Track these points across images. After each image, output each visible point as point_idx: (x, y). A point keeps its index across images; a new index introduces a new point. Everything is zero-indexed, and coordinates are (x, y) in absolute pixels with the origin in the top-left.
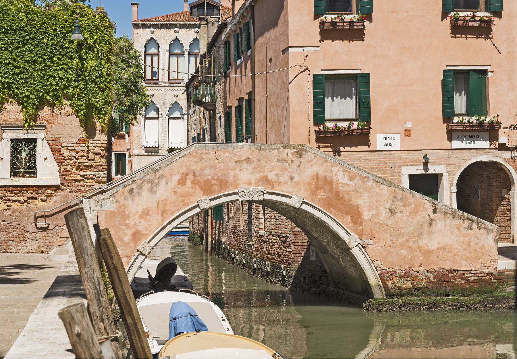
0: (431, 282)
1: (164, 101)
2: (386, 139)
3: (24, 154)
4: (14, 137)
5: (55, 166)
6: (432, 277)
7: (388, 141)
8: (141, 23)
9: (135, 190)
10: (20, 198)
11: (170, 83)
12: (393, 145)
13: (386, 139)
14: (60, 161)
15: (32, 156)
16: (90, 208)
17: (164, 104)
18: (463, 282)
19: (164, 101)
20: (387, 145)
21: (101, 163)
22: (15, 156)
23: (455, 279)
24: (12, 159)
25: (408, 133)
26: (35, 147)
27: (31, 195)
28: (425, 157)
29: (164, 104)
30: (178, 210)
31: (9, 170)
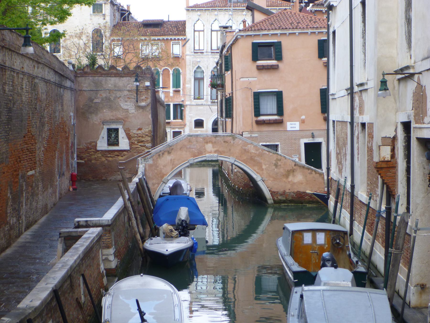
0: (294, 197)
1: (207, 66)
2: (292, 124)
3: (113, 135)
4: (108, 127)
5: (127, 141)
6: (295, 195)
7: (293, 126)
8: (191, 9)
9: (161, 155)
10: (111, 156)
11: (212, 53)
12: (295, 127)
13: (292, 124)
14: (129, 137)
15: (117, 137)
16: (142, 162)
17: (207, 68)
18: (309, 198)
19: (207, 66)
20: (292, 128)
21: (148, 139)
22: (109, 136)
23: (305, 196)
24: (108, 138)
25: (303, 122)
26: (118, 132)
27: (116, 154)
28: (313, 133)
29: (207, 68)
30: (180, 164)
31: (107, 143)
